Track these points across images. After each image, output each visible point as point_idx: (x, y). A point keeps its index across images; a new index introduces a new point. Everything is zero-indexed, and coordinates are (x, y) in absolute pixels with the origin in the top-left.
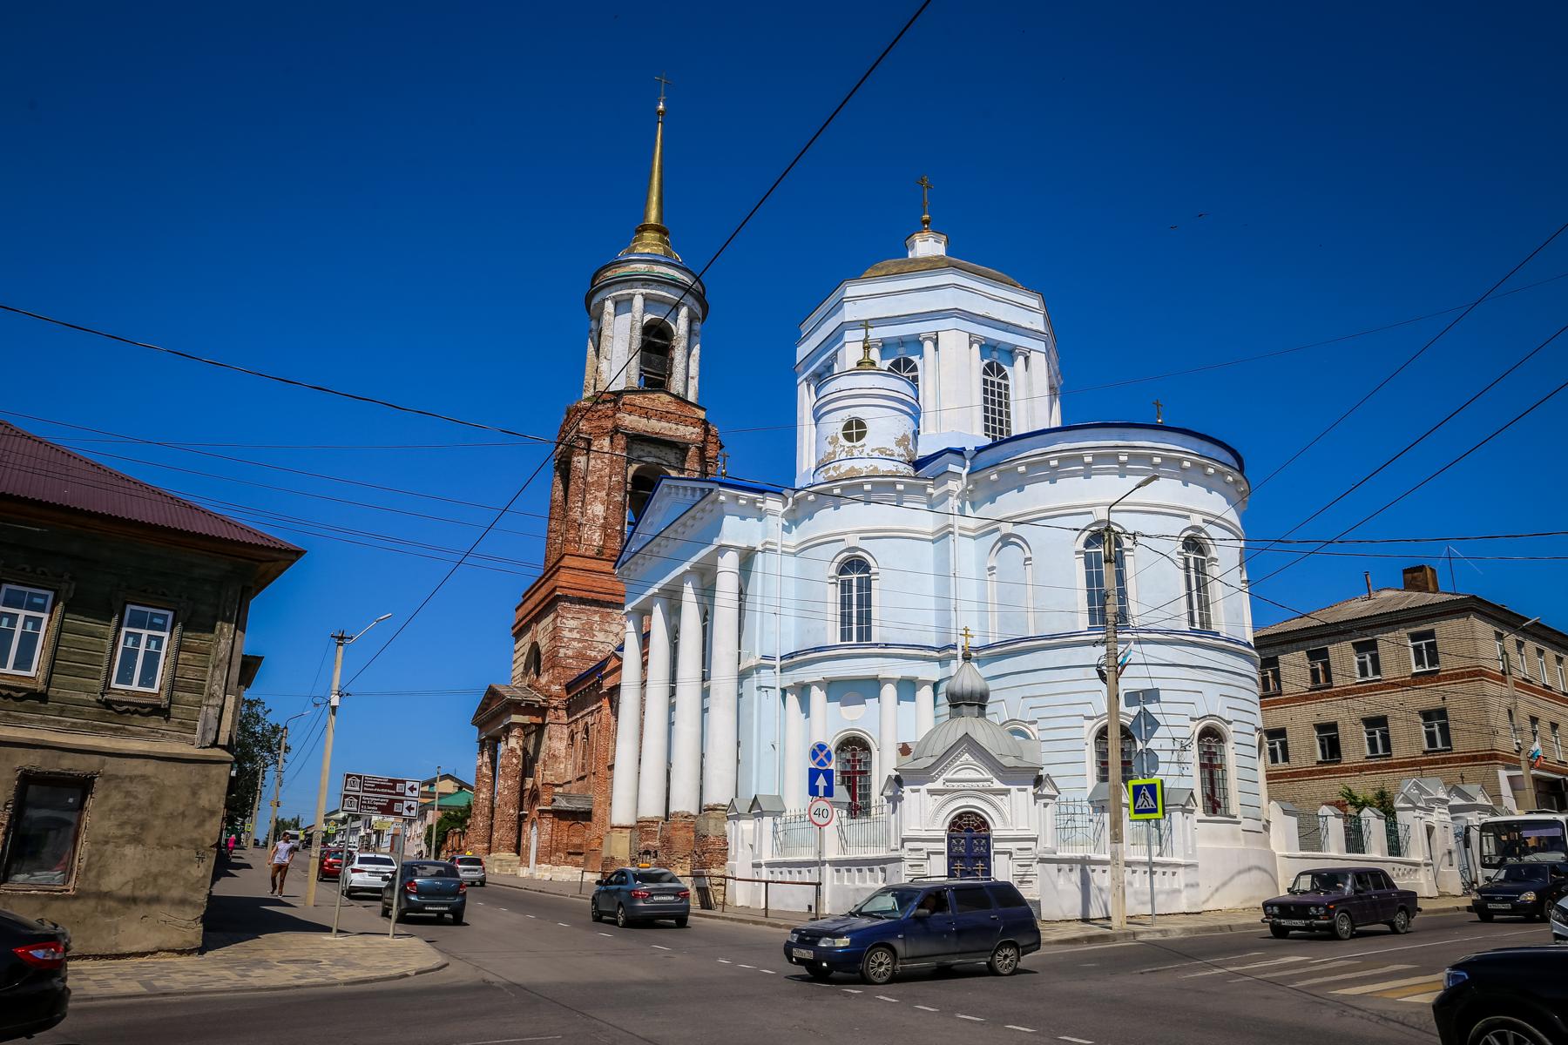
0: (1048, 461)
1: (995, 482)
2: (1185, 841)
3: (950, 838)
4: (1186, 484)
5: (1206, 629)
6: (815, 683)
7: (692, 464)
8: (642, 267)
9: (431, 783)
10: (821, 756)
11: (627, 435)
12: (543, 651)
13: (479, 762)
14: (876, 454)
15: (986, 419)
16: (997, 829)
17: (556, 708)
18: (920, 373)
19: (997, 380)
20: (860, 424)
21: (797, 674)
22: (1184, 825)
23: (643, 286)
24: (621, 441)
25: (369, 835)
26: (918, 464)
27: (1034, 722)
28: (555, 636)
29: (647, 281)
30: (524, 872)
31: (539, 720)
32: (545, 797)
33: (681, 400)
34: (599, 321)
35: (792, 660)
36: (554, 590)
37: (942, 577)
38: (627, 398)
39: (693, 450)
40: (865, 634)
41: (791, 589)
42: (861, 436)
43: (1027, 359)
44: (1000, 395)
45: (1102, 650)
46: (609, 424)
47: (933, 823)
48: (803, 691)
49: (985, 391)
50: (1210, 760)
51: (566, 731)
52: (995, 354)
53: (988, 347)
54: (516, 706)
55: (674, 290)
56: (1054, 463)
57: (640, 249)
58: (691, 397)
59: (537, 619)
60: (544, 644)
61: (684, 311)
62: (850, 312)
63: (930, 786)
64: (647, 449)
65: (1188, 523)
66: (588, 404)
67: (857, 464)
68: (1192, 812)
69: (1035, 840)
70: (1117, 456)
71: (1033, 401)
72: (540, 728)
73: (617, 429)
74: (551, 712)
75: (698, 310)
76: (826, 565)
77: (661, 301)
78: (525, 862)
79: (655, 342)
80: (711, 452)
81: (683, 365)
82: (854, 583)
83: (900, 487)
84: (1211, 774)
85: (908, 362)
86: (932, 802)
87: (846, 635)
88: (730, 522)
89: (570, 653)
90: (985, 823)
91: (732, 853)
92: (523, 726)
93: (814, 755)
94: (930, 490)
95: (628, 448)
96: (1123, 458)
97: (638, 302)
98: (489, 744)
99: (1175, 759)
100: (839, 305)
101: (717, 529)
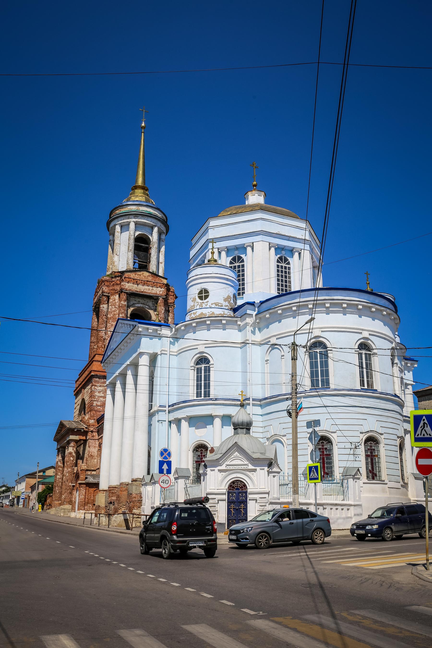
0: (291, 307)
1: (268, 318)
2: (354, 493)
3: (229, 493)
4: (360, 317)
5: (371, 388)
6: (184, 418)
7: (161, 308)
8: (134, 208)
9: (44, 471)
10: (165, 454)
11: (127, 293)
12: (86, 403)
13: (57, 460)
14: (213, 306)
15: (278, 285)
16: (250, 489)
17: (92, 432)
18: (245, 263)
19: (284, 265)
20: (206, 291)
21: (178, 415)
22: (354, 486)
23: (135, 218)
24: (124, 296)
25: (13, 499)
26: (235, 310)
27: (285, 436)
28: (92, 396)
29: (136, 215)
30: (73, 515)
31: (84, 438)
32: (82, 477)
33: (155, 275)
34: (114, 236)
35: (174, 407)
36: (91, 372)
37: (249, 365)
38: (126, 275)
39: (161, 300)
40: (207, 394)
41: (174, 373)
42: (206, 297)
43: (300, 254)
44: (286, 272)
45: (290, 402)
46: (118, 288)
47: (221, 486)
48: (178, 422)
49: (278, 271)
50: (371, 453)
51: (97, 443)
52: (283, 252)
53: (279, 249)
54: (72, 431)
55: (150, 219)
56: (294, 308)
57: (133, 198)
58: (161, 273)
59: (84, 387)
60: (87, 399)
61: (156, 230)
62: (211, 234)
63: (220, 468)
64: (138, 300)
65: (361, 336)
66: (107, 278)
67: (204, 311)
68: (359, 479)
69: (268, 493)
70: (325, 304)
71: (302, 274)
72: (85, 441)
73: (121, 291)
74: (90, 434)
75: (163, 228)
76: (190, 359)
77: (144, 225)
78: (73, 509)
79: (141, 246)
80: (171, 300)
81: (155, 257)
82: (203, 369)
83: (224, 322)
84: (372, 460)
85: (240, 258)
86: (221, 476)
87: (199, 394)
88: (144, 340)
89: (99, 403)
90: (245, 485)
91: (143, 502)
92: (76, 441)
93: (162, 454)
94: (239, 323)
95: (128, 300)
96: (328, 305)
97: (132, 226)
98: (62, 450)
99: (352, 452)
100: (207, 229)
101: (138, 345)
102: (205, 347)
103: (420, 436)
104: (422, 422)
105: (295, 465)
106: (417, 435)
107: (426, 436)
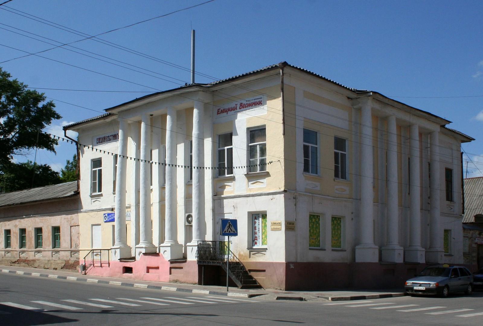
93: (115, 193)
102: (82, 157)
103: (226, 232)
104: (228, 225)
105: (366, 297)
106: (224, 231)
107: (231, 232)
